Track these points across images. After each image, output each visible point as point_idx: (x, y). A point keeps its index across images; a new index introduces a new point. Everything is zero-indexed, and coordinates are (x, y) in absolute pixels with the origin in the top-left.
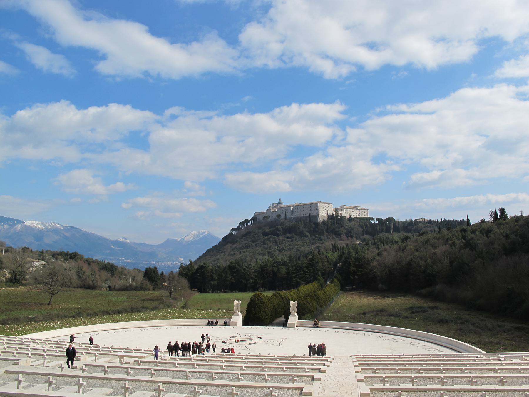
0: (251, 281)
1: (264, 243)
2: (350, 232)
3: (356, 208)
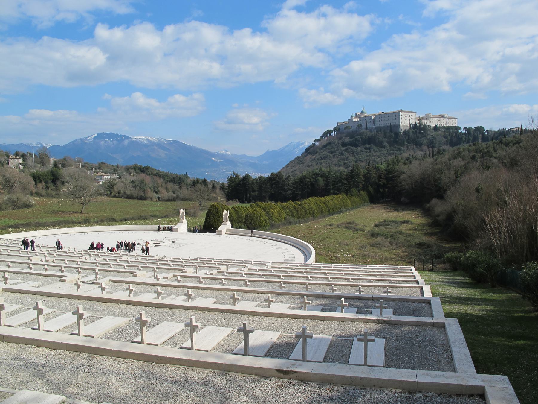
0: (290, 192)
1: (342, 154)
2: (432, 142)
3: (443, 116)
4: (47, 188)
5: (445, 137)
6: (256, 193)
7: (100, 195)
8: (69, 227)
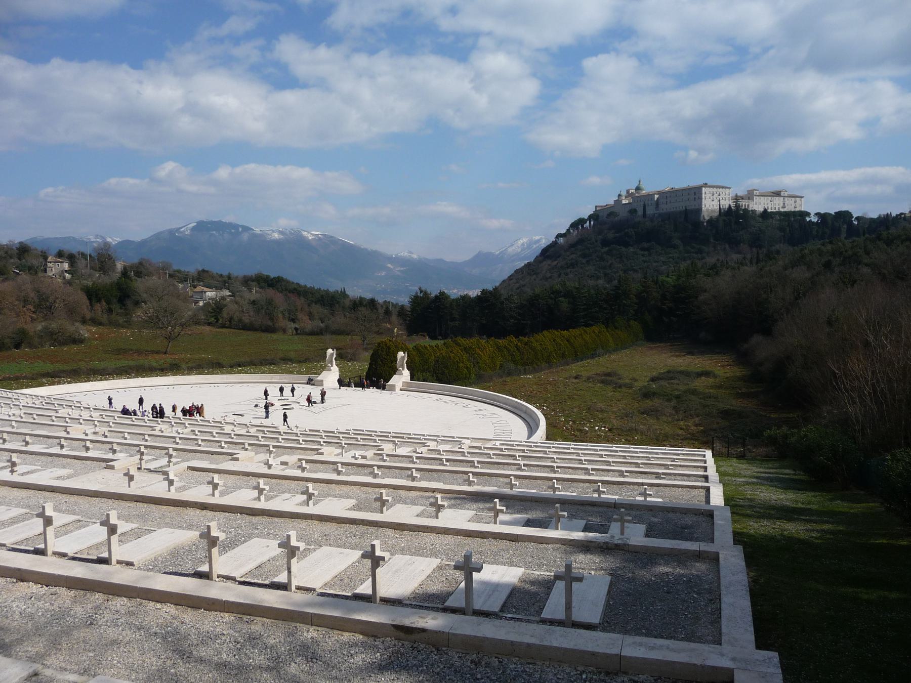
3: (777, 194)
4: (110, 311)
5: (781, 229)
6: (457, 323)
7: (197, 323)
8: (144, 377)
